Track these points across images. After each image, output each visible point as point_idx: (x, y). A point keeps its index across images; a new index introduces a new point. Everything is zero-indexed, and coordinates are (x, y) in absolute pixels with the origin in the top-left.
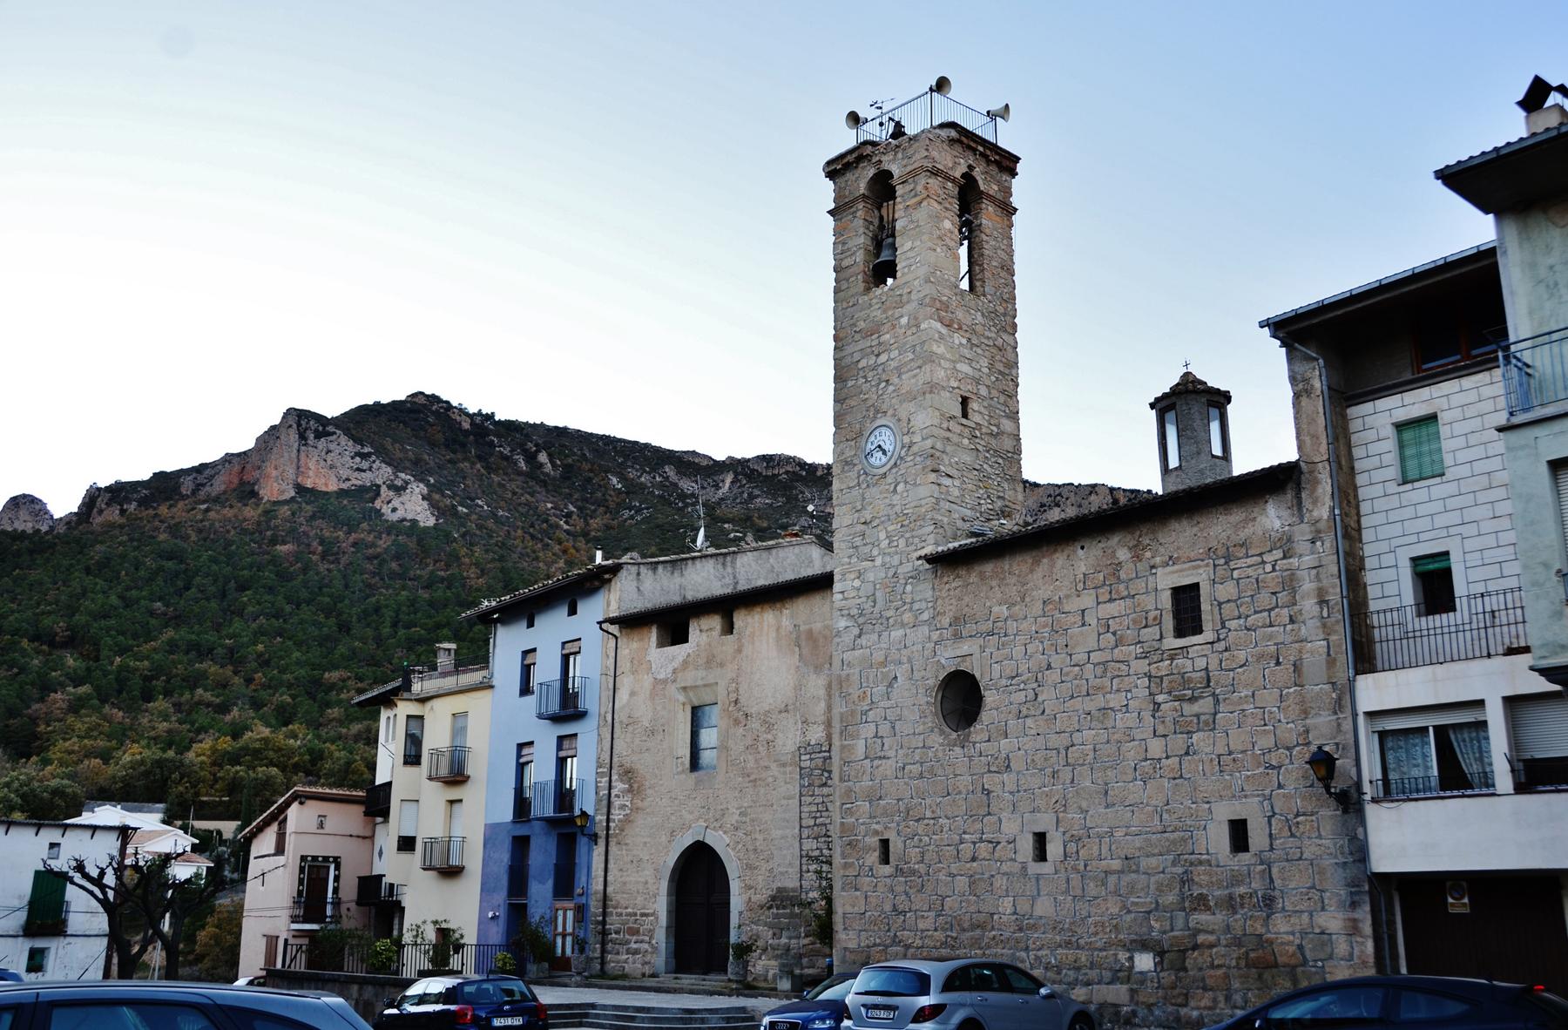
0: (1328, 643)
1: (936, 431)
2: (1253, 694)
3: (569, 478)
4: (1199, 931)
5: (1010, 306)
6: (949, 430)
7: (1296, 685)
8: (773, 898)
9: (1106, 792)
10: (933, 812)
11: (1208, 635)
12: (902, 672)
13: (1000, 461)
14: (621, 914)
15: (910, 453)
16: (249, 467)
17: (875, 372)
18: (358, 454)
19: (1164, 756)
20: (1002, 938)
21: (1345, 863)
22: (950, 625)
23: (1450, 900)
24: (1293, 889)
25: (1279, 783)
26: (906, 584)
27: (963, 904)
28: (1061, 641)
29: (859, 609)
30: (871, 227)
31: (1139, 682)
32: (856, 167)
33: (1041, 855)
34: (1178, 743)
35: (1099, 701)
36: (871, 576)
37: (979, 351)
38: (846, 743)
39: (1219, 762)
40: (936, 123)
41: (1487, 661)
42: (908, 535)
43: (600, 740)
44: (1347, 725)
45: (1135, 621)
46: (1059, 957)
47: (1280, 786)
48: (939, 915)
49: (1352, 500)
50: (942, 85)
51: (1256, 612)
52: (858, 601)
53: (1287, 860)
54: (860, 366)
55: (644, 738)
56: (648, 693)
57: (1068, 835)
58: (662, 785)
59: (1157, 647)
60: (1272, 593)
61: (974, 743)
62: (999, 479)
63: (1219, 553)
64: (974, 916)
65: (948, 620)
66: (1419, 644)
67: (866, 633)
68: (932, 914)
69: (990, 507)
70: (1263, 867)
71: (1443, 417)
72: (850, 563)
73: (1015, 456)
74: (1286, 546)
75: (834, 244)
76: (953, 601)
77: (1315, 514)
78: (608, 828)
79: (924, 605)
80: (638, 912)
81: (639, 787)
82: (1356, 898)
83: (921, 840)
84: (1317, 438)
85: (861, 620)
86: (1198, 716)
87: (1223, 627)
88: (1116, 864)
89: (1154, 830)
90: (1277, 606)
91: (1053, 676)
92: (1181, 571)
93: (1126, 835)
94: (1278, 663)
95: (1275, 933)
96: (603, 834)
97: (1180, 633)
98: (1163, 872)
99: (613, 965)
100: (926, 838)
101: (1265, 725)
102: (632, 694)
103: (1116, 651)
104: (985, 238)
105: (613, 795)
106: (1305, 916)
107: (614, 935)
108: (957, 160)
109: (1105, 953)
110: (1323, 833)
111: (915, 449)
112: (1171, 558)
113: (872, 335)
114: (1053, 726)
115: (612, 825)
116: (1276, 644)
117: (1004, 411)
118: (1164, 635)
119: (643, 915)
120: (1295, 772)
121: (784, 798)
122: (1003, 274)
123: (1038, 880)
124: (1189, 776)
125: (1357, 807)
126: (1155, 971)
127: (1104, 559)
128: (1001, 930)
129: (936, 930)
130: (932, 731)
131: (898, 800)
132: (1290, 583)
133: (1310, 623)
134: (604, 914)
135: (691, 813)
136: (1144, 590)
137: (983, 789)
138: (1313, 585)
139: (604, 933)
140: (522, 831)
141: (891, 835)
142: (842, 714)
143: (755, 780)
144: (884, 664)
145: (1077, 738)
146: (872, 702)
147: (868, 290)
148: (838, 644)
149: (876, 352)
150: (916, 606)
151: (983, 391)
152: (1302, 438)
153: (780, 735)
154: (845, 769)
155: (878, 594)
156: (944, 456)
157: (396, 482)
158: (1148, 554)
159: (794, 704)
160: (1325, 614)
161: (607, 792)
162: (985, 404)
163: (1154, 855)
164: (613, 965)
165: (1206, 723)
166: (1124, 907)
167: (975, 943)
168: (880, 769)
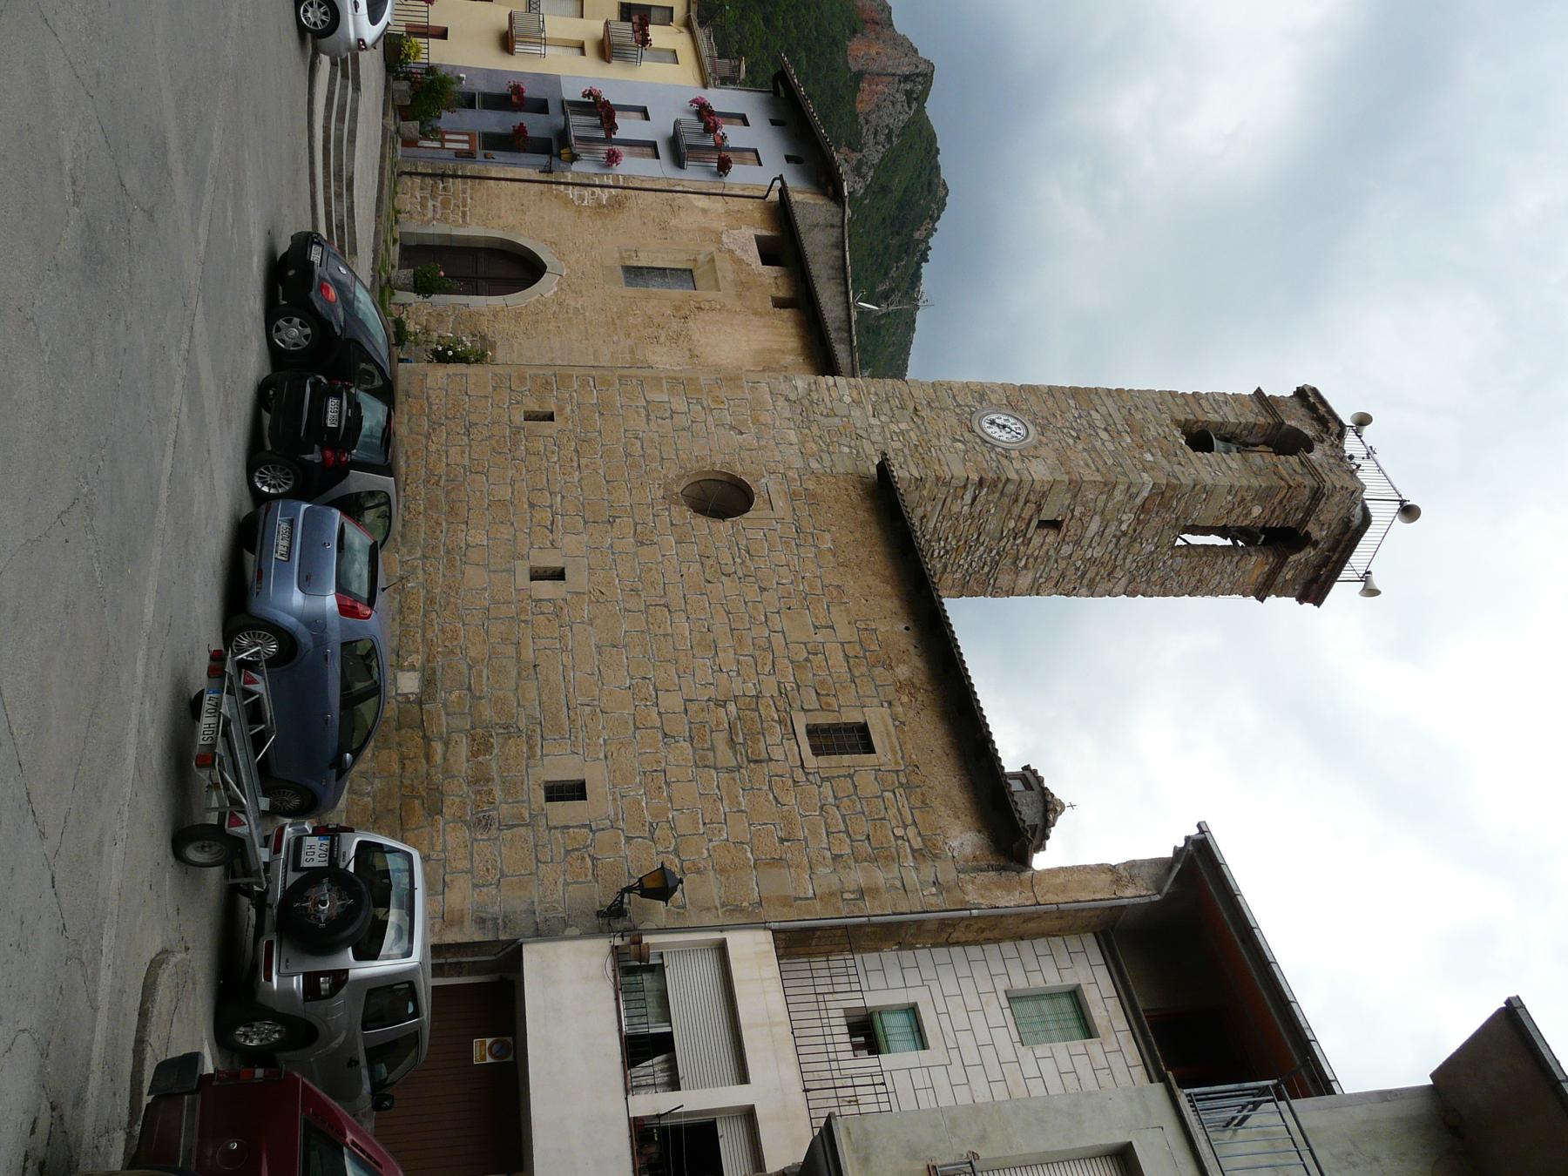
0: (811, 898)
1: (1026, 488)
2: (742, 811)
3: (868, 332)
4: (446, 744)
5: (1157, 589)
6: (1027, 502)
7: (755, 860)
8: (483, 338)
9: (615, 646)
10: (587, 466)
11: (812, 761)
12: (749, 438)
13: (986, 569)
14: (464, 192)
15: (1000, 457)
16: (878, 28)
17: (1087, 426)
18: (891, 131)
19: (662, 711)
20: (438, 532)
21: (535, 913)
22: (806, 489)
23: (489, 1041)
24: (500, 852)
25: (632, 838)
26: (850, 447)
27: (478, 494)
28: (794, 603)
29: (818, 400)
30: (1245, 433)
31: (750, 685)
32: (1313, 418)
33: (537, 575)
34: (681, 727)
35: (725, 642)
36: (856, 413)
37: (1111, 546)
38: (665, 384)
39: (656, 771)
40: (1370, 505)
41: (798, 1089)
42: (906, 451)
43: (653, 179)
44: (708, 920)
45: (823, 682)
46: (415, 591)
47: (629, 839)
48: (465, 469)
49: (983, 935)
50: (1409, 512)
51: (843, 817)
52: (827, 400)
53: (536, 846)
54: (1092, 412)
55: (657, 220)
56: (706, 225)
57: (562, 603)
58: (606, 235)
59: (794, 705)
60: (868, 836)
61: (669, 510)
62: (966, 566)
63: (912, 777)
64: (465, 504)
65: (811, 487)
66: (810, 1014)
67: (790, 405)
68: (467, 462)
69: (936, 554)
70: (527, 815)
71: (1093, 1045)
72: (869, 393)
73: (990, 589)
74: (927, 853)
75: (1224, 393)
76: (833, 492)
77: (970, 887)
78: (560, 183)
79: (827, 464)
80: (467, 209)
81: (604, 213)
82: (489, 924)
83: (553, 453)
84: (1063, 892)
85: (806, 402)
86: (712, 748)
87: (823, 780)
88: (528, 654)
89: (571, 696)
90: (852, 841)
91: (752, 593)
92: (888, 735)
93: (564, 666)
94: (782, 840)
95: (444, 830)
96: (552, 178)
97: (812, 731)
98: (519, 705)
99: (409, 184)
100: (556, 459)
101: (704, 824)
102: (704, 211)
103: (786, 661)
104: (1235, 559)
105: (594, 189)
106: (465, 864)
107: (441, 185)
108: (1326, 526)
109: (419, 640)
110: (570, 888)
111: (1005, 462)
112: (903, 723)
113: (1127, 424)
114: (692, 592)
115: (562, 187)
116: (806, 839)
117: (1041, 577)
118: (808, 713)
119: (464, 214)
120: (642, 860)
121: (595, 351)
122: (1193, 581)
123: (508, 571)
124: (638, 737)
125: (606, 928)
126: (397, 694)
127: (896, 652)
128: (448, 531)
129: (448, 465)
130: (681, 467)
131: (600, 432)
132: (883, 856)
133: (834, 878)
134: (464, 177)
135: (577, 262)
136: (861, 693)
137: (615, 517)
138: (881, 881)
139: (443, 176)
140: (553, 107)
141: (558, 423)
142: (698, 378)
143: (614, 323)
144: (756, 421)
145: (680, 618)
146: (711, 410)
147: (1178, 423)
148: (777, 379)
149: (1109, 428)
150: (825, 456)
151: (1066, 550)
152: (1062, 874)
153: (666, 349)
154: (634, 381)
155: (837, 420)
156: (997, 495)
157: (865, 167)
158: (905, 699)
159: (700, 364)
160: (846, 896)
161: (597, 183)
162: (1052, 552)
163: (540, 695)
164: (409, 184)
165: (703, 758)
166: (475, 661)
167: (432, 504)
168: (636, 416)
